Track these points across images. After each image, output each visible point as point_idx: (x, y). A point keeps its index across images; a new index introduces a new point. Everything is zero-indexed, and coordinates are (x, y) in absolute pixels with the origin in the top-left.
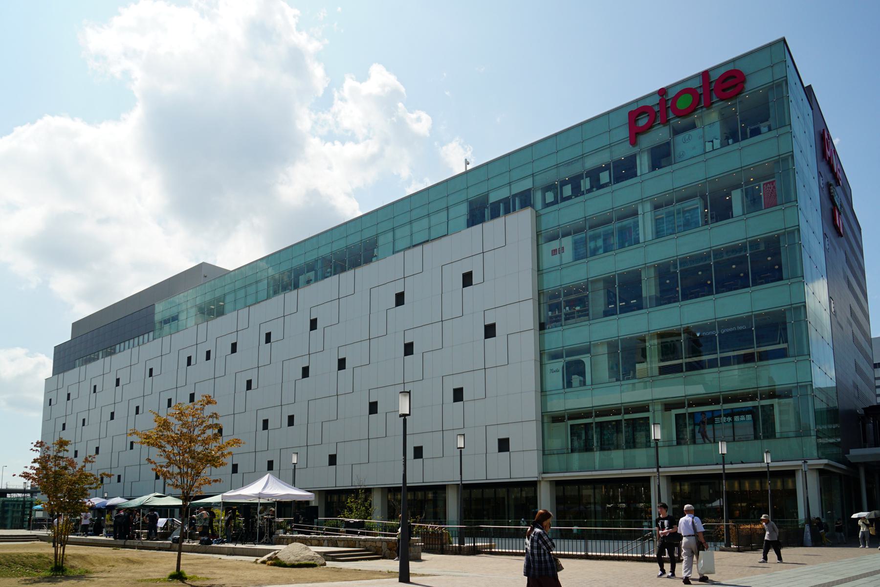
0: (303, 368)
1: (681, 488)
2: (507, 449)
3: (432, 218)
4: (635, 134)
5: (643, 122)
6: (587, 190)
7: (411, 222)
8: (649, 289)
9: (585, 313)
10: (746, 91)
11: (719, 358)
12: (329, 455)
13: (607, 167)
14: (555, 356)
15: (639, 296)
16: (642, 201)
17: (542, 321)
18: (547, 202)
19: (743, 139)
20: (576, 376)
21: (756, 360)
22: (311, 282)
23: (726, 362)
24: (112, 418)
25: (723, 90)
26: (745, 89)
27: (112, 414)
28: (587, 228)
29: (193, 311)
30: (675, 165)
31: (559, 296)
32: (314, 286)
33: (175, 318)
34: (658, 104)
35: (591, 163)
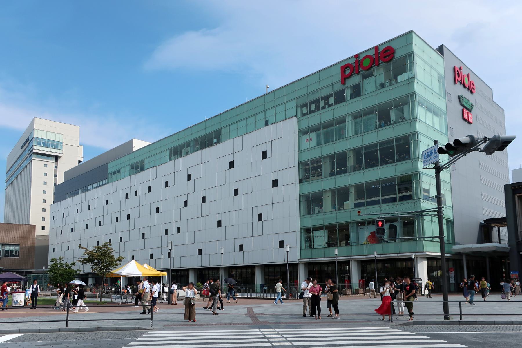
0: (128, 215)
1: (405, 264)
2: (242, 250)
3: (277, 108)
4: (344, 79)
5: (348, 72)
8: (350, 162)
9: (320, 175)
12: (198, 249)
16: (348, 115)
17: (301, 178)
20: (317, 208)
22: (189, 153)
23: (384, 201)
24: (87, 228)
25: (385, 57)
27: (87, 225)
29: (128, 168)
30: (363, 96)
31: (308, 165)
32: (189, 156)
33: (119, 171)
34: (374, 54)
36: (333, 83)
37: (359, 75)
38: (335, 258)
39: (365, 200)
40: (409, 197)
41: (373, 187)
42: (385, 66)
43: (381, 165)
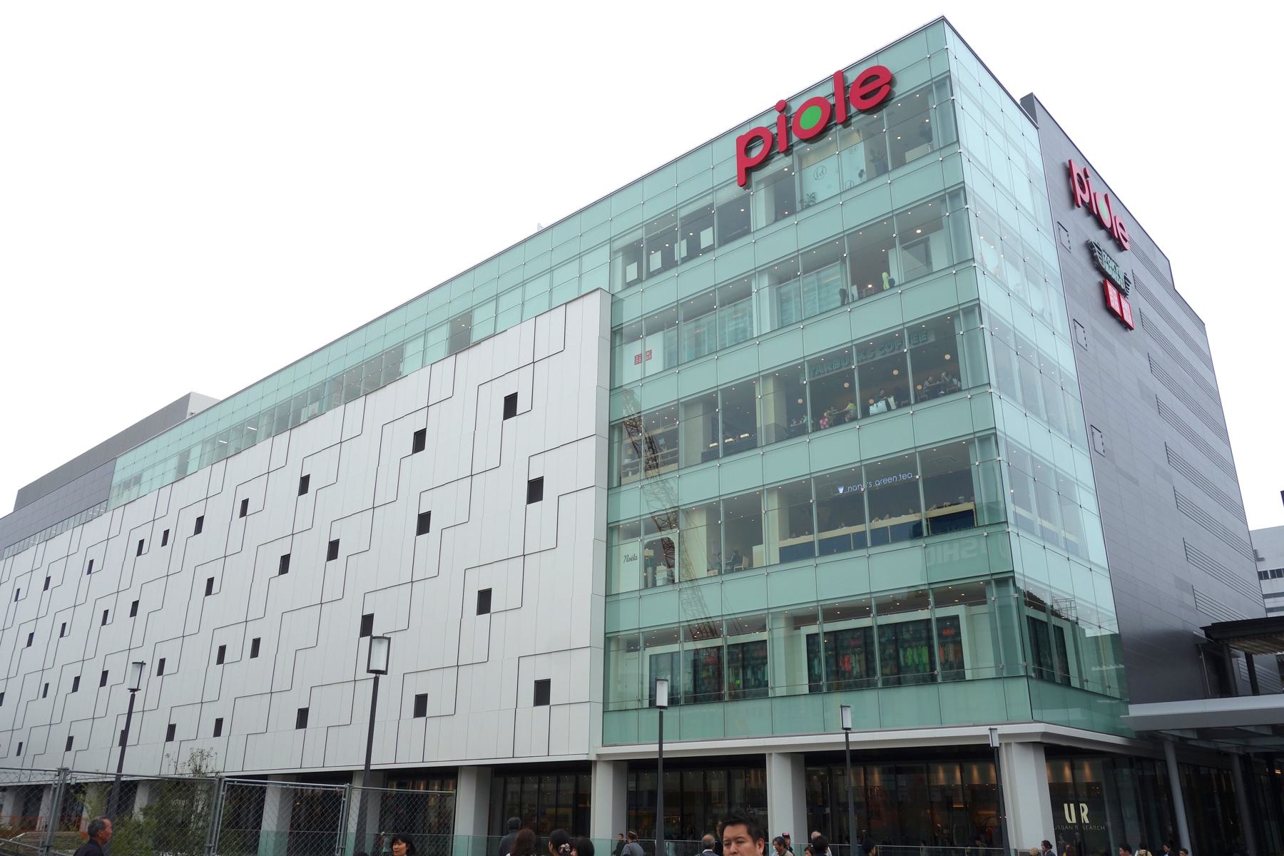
4: (746, 173)
5: (756, 152)
6: (682, 259)
8: (767, 413)
10: (896, 95)
12: (535, 681)
14: (633, 533)
15: (752, 429)
16: (759, 272)
18: (627, 281)
19: (895, 167)
21: (925, 534)
23: (880, 538)
26: (895, 94)
28: (681, 317)
36: (713, 187)
37: (791, 156)
38: (842, 738)
39: (814, 538)
40: (964, 521)
41: (841, 490)
42: (867, 125)
43: (916, 402)
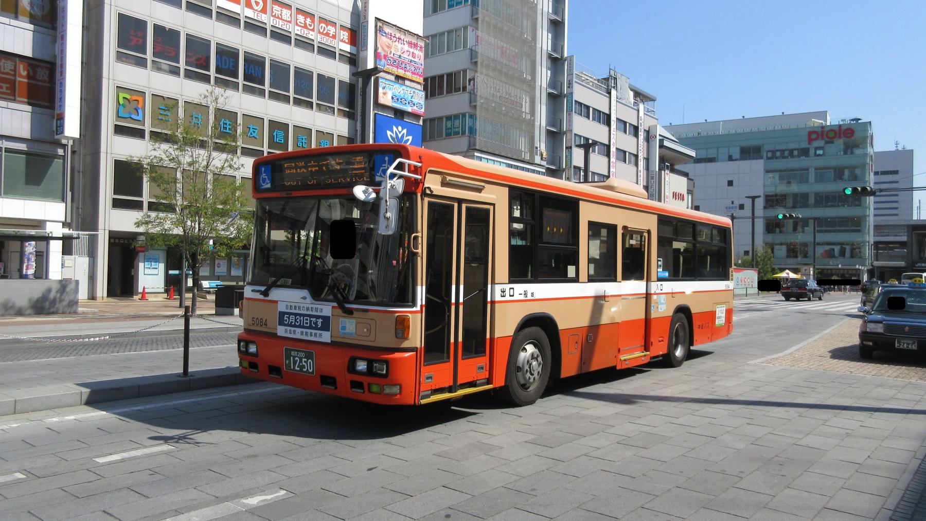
4: (810, 140)
5: (814, 136)
7: (707, 149)
8: (812, 200)
11: (824, 197)
13: (798, 149)
35: (791, 146)
